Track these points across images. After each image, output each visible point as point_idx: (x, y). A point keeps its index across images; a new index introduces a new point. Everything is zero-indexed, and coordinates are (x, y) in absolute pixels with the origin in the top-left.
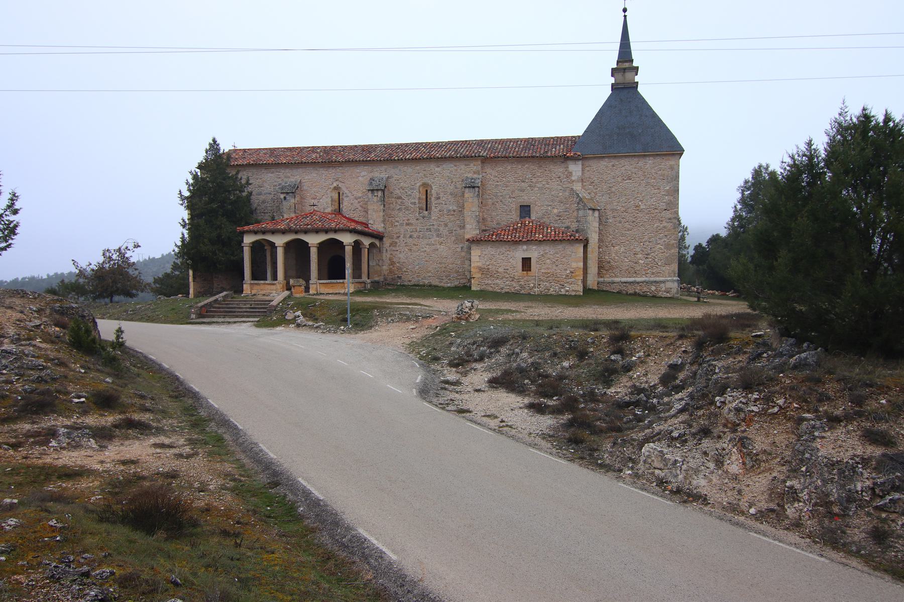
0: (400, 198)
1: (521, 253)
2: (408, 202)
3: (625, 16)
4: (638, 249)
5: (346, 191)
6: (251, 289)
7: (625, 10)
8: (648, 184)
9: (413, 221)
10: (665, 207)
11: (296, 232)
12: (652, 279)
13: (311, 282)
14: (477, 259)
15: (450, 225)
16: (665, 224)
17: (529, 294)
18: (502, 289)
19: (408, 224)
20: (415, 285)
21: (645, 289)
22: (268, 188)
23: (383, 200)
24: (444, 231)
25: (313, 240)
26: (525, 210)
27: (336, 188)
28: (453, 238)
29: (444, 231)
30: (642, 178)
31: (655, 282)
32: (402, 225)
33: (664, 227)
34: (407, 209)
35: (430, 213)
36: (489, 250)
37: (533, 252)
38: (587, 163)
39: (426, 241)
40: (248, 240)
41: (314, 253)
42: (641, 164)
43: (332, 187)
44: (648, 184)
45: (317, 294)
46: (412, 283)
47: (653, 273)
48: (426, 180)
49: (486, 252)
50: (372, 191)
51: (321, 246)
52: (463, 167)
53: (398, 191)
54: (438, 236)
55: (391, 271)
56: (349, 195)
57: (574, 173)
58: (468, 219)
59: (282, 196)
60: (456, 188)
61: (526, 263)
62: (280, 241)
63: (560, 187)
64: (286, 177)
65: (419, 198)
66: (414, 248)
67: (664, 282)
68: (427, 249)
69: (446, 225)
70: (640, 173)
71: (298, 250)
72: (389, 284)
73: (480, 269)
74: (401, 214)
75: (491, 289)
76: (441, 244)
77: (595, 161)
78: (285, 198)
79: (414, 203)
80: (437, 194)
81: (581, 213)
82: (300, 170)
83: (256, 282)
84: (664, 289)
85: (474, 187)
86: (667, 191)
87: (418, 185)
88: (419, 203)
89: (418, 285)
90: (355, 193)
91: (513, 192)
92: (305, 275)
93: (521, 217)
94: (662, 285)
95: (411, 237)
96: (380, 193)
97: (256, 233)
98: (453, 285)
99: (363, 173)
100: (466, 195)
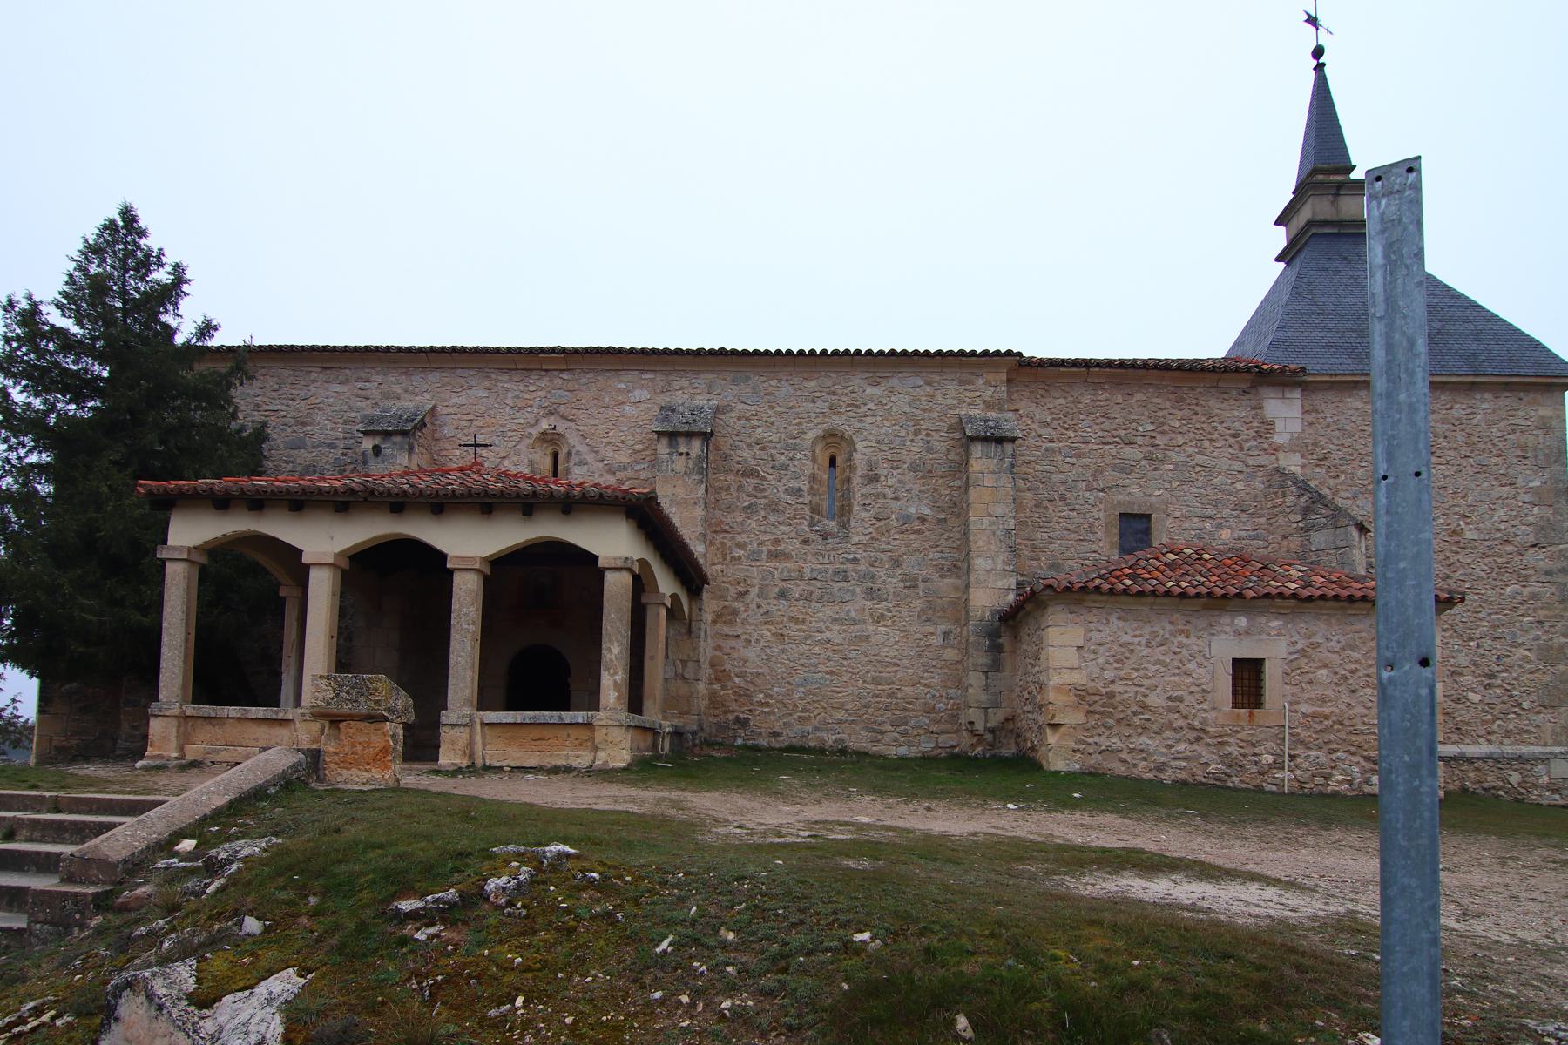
0: (751, 473)
1: (1228, 641)
2: (777, 489)
3: (1320, 68)
4: (1463, 660)
5: (583, 449)
6: (184, 740)
7: (1318, 52)
8: (1481, 468)
9: (793, 547)
10: (1531, 539)
11: (398, 504)
12: (1509, 750)
13: (447, 717)
14: (1072, 657)
15: (909, 562)
16: (1537, 588)
17: (1259, 790)
18: (1160, 769)
19: (774, 556)
20: (791, 748)
21: (1491, 780)
22: (325, 426)
23: (703, 469)
24: (891, 581)
25: (468, 544)
26: (1135, 527)
27: (550, 439)
28: (918, 604)
29: (891, 581)
30: (1465, 451)
31: (1521, 758)
32: (755, 556)
33: (1535, 596)
34: (773, 507)
35: (845, 525)
36: (1115, 628)
37: (1273, 643)
38: (1318, 399)
39: (831, 611)
40: (189, 533)
41: (467, 595)
42: (1460, 409)
43: (535, 432)
44: (1481, 468)
45: (472, 770)
46: (783, 742)
47: (1508, 733)
48: (834, 422)
49: (1105, 636)
50: (672, 436)
51: (502, 571)
52: (951, 387)
53: (747, 454)
54: (870, 594)
55: (715, 702)
56: (590, 457)
57: (1279, 426)
58: (979, 541)
59: (368, 444)
60: (930, 450)
61: (1248, 678)
62: (323, 542)
63: (1237, 465)
64: (386, 396)
65: (813, 478)
66: (793, 631)
67: (1544, 759)
68: (835, 635)
69: (896, 563)
70: (1460, 436)
71: (394, 589)
72: (711, 744)
73: (1082, 695)
74: (752, 524)
75: (1121, 769)
76: (879, 619)
77: (1330, 396)
78: (377, 450)
79: (798, 493)
80: (871, 466)
81: (1319, 539)
82: (434, 377)
83: (207, 710)
84: (1544, 780)
85: (999, 441)
86: (1536, 491)
87: (810, 435)
88: (812, 491)
89: (802, 750)
90: (608, 453)
91: (1098, 471)
92: (425, 677)
93: (1125, 550)
94: (1540, 769)
95: (783, 595)
96: (696, 447)
97: (222, 503)
98: (914, 752)
99: (638, 394)
100: (976, 465)
